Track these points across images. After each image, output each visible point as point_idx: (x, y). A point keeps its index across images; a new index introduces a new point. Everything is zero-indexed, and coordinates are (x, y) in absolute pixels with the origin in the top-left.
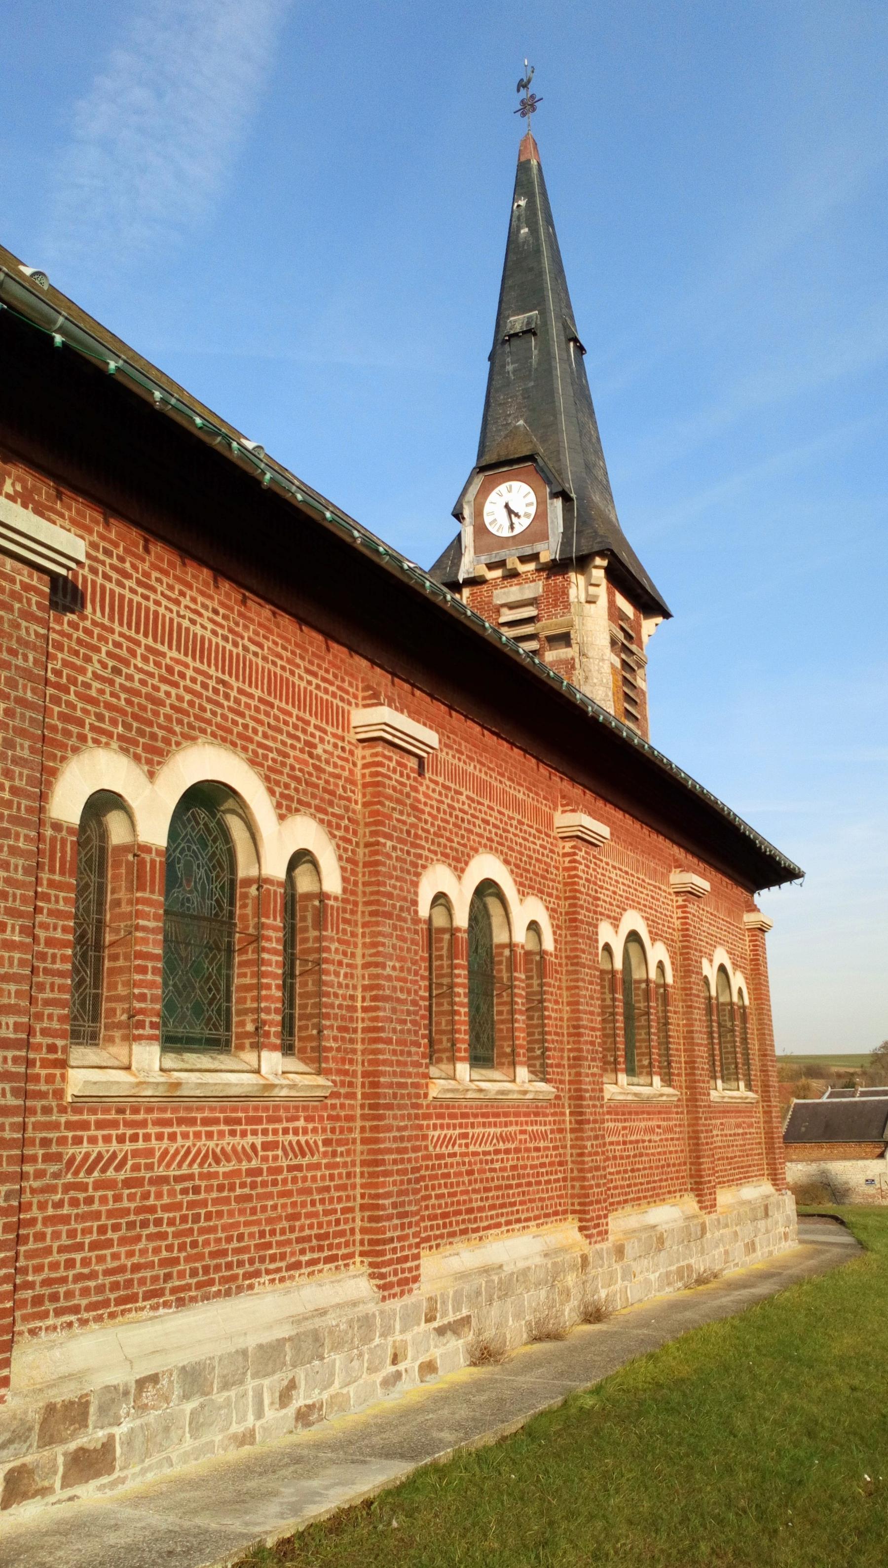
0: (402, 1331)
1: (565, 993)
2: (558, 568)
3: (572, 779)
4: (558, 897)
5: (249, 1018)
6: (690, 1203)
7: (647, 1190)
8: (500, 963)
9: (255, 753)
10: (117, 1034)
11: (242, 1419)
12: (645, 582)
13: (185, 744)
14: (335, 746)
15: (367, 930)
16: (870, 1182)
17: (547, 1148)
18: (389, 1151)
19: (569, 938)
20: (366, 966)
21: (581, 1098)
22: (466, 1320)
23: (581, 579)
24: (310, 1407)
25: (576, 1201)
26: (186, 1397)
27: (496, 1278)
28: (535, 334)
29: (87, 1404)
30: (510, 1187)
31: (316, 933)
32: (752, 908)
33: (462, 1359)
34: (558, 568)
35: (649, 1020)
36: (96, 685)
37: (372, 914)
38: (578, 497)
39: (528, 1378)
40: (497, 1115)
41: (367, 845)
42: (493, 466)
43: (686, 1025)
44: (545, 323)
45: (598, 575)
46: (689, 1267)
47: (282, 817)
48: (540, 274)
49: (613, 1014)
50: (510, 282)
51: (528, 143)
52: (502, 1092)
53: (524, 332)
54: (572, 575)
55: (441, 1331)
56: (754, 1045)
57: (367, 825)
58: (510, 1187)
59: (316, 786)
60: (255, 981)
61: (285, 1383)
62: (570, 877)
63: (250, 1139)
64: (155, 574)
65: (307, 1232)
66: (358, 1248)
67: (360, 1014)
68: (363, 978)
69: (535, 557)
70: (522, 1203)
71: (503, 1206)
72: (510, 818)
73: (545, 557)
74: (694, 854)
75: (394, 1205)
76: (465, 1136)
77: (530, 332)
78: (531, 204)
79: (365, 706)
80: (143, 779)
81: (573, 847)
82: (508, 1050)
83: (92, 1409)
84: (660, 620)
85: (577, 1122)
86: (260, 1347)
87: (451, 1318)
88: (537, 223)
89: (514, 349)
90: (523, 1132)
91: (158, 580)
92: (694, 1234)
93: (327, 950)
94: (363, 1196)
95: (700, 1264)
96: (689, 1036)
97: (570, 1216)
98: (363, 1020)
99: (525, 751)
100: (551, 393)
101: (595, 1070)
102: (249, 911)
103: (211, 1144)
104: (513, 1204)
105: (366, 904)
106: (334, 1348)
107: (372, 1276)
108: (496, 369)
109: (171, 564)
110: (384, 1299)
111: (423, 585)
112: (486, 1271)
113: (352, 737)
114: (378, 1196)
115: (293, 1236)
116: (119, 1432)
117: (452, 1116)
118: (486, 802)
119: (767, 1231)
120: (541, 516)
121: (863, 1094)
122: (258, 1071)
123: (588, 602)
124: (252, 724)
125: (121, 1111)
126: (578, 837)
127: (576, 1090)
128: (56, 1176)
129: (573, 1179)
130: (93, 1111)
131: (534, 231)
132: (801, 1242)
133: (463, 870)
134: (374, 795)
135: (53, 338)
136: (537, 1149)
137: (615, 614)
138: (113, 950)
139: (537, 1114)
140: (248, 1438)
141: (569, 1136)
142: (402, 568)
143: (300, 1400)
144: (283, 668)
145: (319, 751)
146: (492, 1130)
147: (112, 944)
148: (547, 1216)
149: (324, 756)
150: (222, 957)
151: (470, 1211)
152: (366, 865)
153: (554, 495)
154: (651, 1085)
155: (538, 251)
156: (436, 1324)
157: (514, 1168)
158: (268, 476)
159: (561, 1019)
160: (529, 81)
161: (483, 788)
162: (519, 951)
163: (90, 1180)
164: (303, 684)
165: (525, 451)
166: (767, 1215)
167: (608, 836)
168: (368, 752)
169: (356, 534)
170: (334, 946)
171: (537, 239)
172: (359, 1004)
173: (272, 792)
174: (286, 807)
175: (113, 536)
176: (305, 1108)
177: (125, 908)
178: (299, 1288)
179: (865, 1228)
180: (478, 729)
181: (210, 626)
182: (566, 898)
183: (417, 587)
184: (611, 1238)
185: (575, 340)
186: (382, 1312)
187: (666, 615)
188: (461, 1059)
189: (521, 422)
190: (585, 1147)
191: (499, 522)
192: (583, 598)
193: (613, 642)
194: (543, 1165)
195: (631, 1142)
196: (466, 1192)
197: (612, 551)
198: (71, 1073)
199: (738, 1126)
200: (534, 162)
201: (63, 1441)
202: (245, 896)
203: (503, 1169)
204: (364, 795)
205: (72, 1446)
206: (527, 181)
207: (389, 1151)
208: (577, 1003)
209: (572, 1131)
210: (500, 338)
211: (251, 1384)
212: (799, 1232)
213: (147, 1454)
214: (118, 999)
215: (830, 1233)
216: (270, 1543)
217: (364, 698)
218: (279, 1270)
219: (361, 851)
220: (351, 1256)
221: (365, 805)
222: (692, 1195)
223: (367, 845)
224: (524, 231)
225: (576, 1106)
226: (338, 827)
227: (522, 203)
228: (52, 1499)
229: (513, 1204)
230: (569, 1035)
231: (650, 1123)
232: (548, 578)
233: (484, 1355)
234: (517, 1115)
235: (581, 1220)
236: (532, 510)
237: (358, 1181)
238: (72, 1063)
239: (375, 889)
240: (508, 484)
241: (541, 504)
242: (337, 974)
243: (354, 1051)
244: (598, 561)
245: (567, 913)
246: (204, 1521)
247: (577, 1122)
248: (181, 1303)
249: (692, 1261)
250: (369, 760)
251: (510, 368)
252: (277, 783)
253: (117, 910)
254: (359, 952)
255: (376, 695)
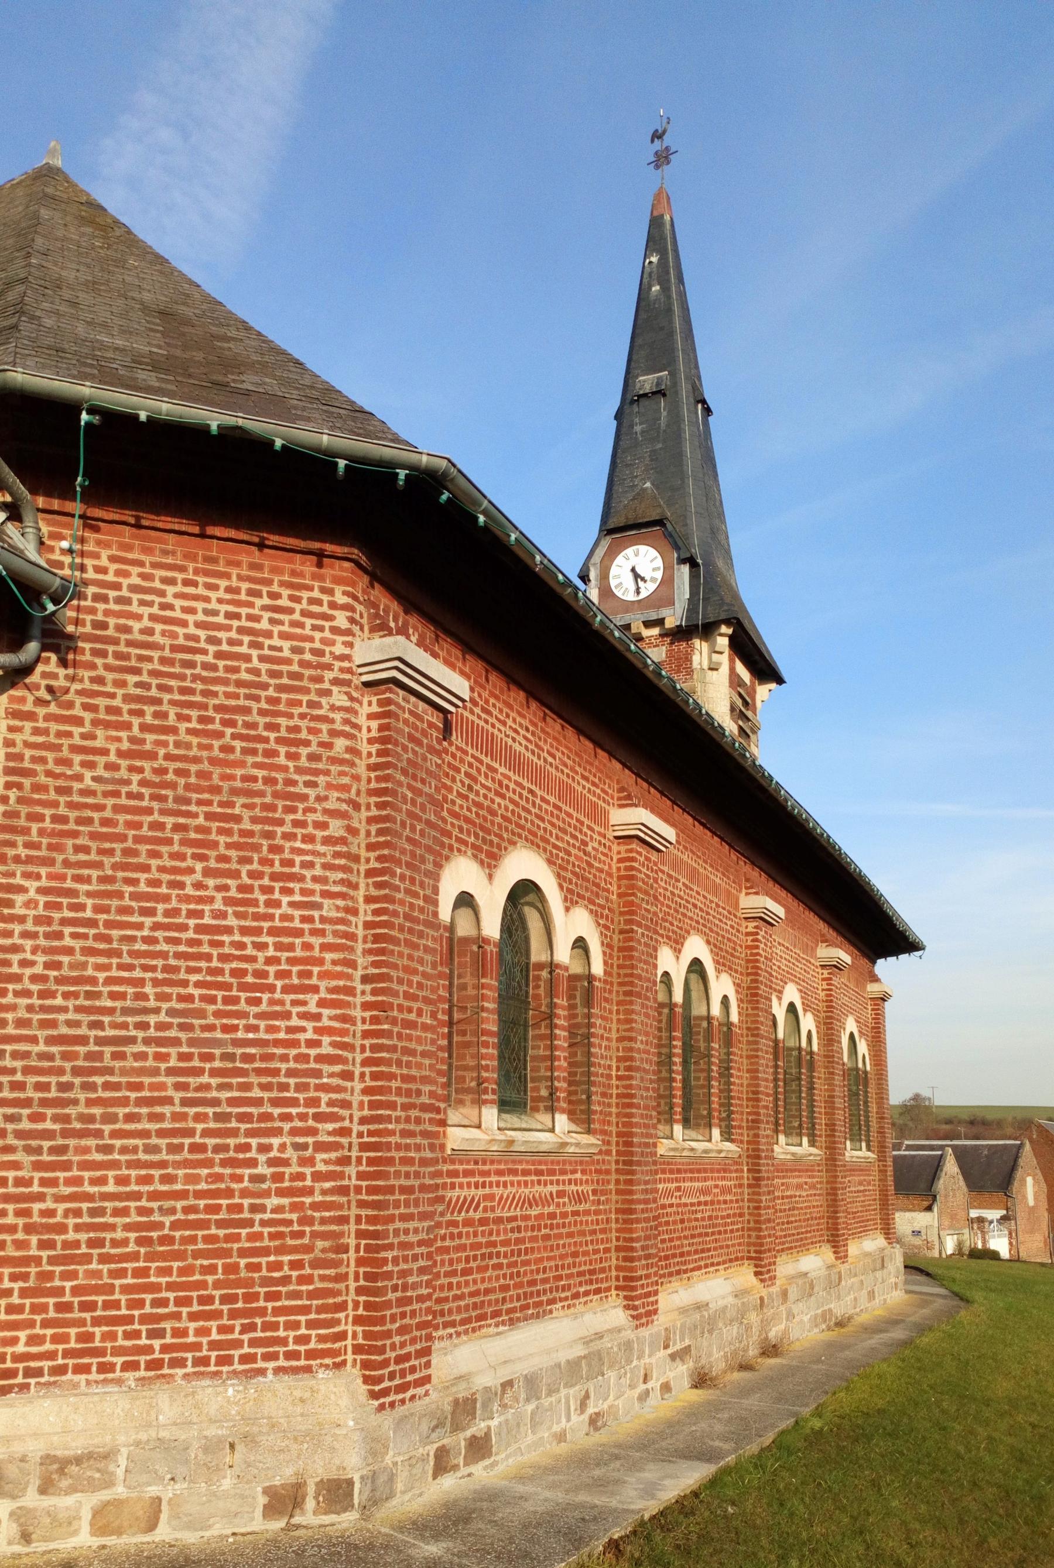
0: (650, 1356)
1: (745, 1061)
2: (682, 634)
3: (753, 863)
4: (742, 974)
5: (543, 1085)
6: (827, 1254)
7: (797, 1241)
8: (698, 1033)
9: (551, 853)
10: (468, 1098)
11: (559, 1422)
12: (761, 646)
13: (510, 848)
14: (600, 843)
15: (621, 1008)
16: (916, 1233)
17: (731, 1201)
18: (639, 1202)
19: (750, 1011)
20: (620, 1039)
21: (759, 1157)
22: (687, 1350)
23: (705, 646)
24: (597, 1414)
25: (752, 1249)
26: (528, 1400)
27: (706, 1314)
28: (664, 395)
29: (475, 1401)
30: (707, 1234)
31: (586, 1011)
32: (875, 979)
33: (686, 1383)
34: (682, 634)
35: (800, 1085)
36: (459, 801)
37: (626, 993)
38: (701, 561)
39: (750, 1401)
40: (699, 1171)
41: (621, 932)
42: (619, 528)
43: (748, 1075)
44: (675, 384)
45: (723, 642)
46: (830, 1310)
47: (567, 909)
48: (671, 334)
49: (670, 1056)
50: (639, 341)
51: (661, 197)
52: (705, 1151)
53: (653, 393)
54: (697, 642)
55: (673, 1357)
56: (873, 1108)
57: (621, 913)
58: (707, 1234)
59: (588, 880)
60: (548, 1053)
61: (583, 1393)
62: (752, 954)
63: (549, 1188)
64: (492, 701)
65: (583, 1268)
66: (614, 1283)
67: (614, 1082)
68: (618, 1050)
69: (660, 622)
70: (715, 1249)
71: (703, 1251)
72: (711, 902)
73: (670, 623)
74: (835, 929)
75: (643, 1248)
76: (678, 1189)
77: (660, 393)
78: (663, 262)
79: (621, 806)
80: (486, 881)
81: (756, 927)
82: (705, 1113)
83: (478, 1405)
84: (773, 686)
85: (755, 1179)
86: (568, 1361)
87: (679, 1346)
88: (669, 281)
89: (642, 410)
90: (716, 1186)
91: (494, 706)
92: (834, 1283)
93: (594, 1025)
94: (618, 1239)
95: (839, 1308)
96: (830, 1101)
97: (746, 1262)
98: (617, 1087)
99: (722, 839)
100: (680, 455)
101: (768, 1132)
102: (541, 991)
103: (527, 1191)
104: (709, 1250)
105: (620, 984)
106: (611, 1367)
107: (627, 1307)
108: (624, 430)
109: (502, 692)
110: (637, 1327)
111: (687, 702)
112: (699, 1308)
113: (610, 835)
114: (632, 1240)
115: (575, 1271)
116: (494, 1423)
117: (671, 1172)
118: (695, 888)
119: (883, 1282)
120: (667, 581)
121: (909, 1148)
122: (552, 1130)
123: (711, 669)
124: (549, 827)
125: (476, 1163)
126: (761, 918)
127: (754, 1150)
128: (442, 1214)
129: (749, 1229)
130: (461, 1163)
131: (665, 289)
132: (907, 1292)
133: (680, 951)
134: (628, 887)
135: (477, 518)
136: (725, 1202)
137: (735, 681)
138: (462, 1027)
139: (725, 1171)
140: (561, 1437)
141: (746, 1191)
142: (675, 687)
143: (591, 1410)
144: (568, 776)
145: (589, 849)
146: (696, 1184)
147: (459, 1022)
148: (731, 1261)
149: (593, 853)
150: (521, 1030)
151: (682, 1255)
152: (620, 949)
153: (682, 561)
154: (800, 1145)
155: (669, 310)
156: (670, 1351)
157: (710, 1218)
158: (598, 619)
159: (742, 1085)
160: (664, 132)
161: (693, 875)
162: (716, 1023)
163: (460, 1219)
164: (580, 789)
165: (654, 516)
166: (883, 1266)
167: (783, 916)
168: (623, 848)
169: (649, 662)
170: (599, 1022)
171: (669, 297)
172: (614, 1073)
173: (561, 887)
174: (570, 901)
175: (467, 670)
176: (581, 1163)
177: (471, 992)
178: (582, 1314)
179: (954, 1280)
180: (691, 820)
181: (524, 742)
182: (748, 974)
183: (681, 704)
184: (778, 1282)
185: (704, 402)
186: (638, 1338)
187: (780, 681)
188: (677, 1121)
189: (648, 485)
190: (761, 1201)
191: (625, 586)
192: (705, 665)
193: (733, 709)
194: (728, 1216)
195: (788, 1197)
196: (679, 1238)
197: (738, 619)
198: (450, 1130)
199: (860, 1183)
200: (667, 218)
201: (463, 1429)
202: (538, 978)
203: (703, 1219)
204: (619, 887)
205: (468, 1433)
206: (659, 237)
207: (639, 1202)
208: (757, 1071)
209: (749, 1186)
210: (629, 397)
211: (563, 1392)
212: (906, 1282)
213: (508, 1445)
214: (466, 1068)
215: (920, 1284)
216: (647, 1517)
217: (619, 799)
218: (566, 1299)
219: (616, 937)
220: (608, 1289)
221: (620, 895)
222: (828, 1246)
223: (621, 932)
224: (656, 288)
225: (754, 1164)
226: (602, 917)
227: (654, 259)
228: (459, 1474)
229: (709, 1250)
230: (748, 1099)
231: (800, 1180)
232: (672, 643)
233: (701, 1380)
234: (712, 1171)
235: (756, 1266)
236: (659, 575)
237: (614, 1226)
238: (449, 1122)
239: (629, 971)
240: (635, 548)
241: (668, 568)
242: (600, 1047)
243: (610, 1114)
244: (724, 629)
245: (748, 988)
246: (583, 1497)
247: (755, 1179)
248: (512, 1322)
249: (832, 1306)
250: (623, 855)
251: (638, 428)
252: (564, 879)
253: (464, 993)
254: (614, 1026)
255: (629, 797)
